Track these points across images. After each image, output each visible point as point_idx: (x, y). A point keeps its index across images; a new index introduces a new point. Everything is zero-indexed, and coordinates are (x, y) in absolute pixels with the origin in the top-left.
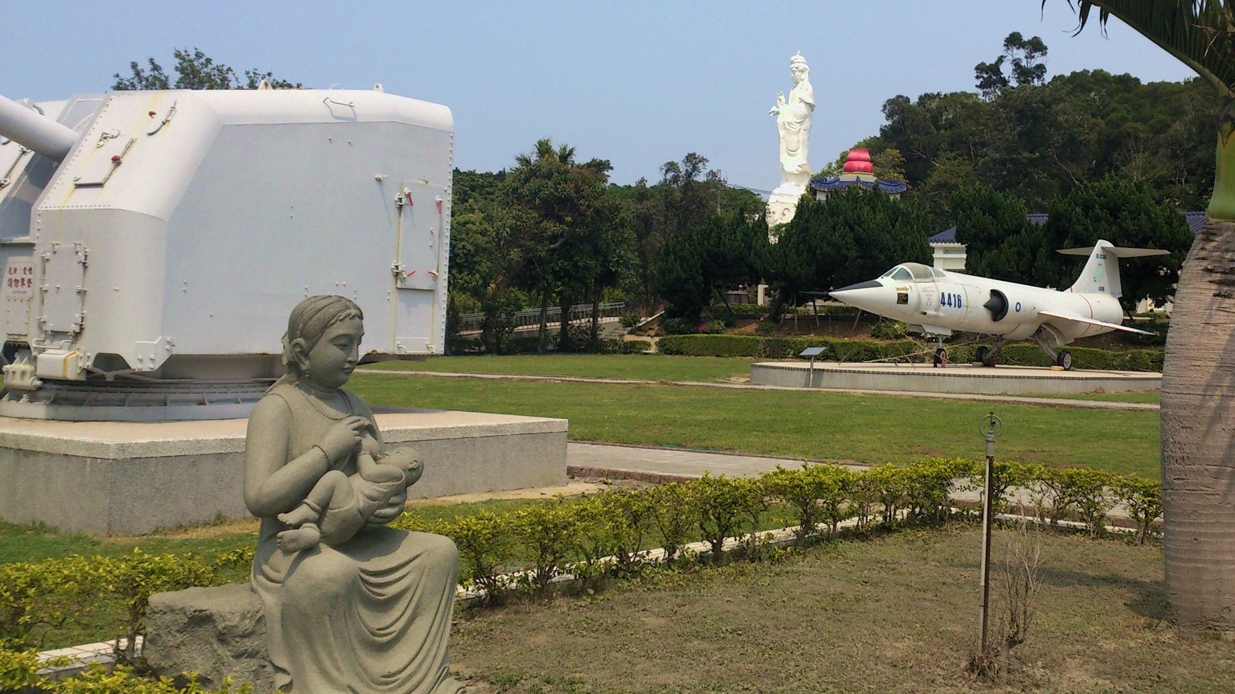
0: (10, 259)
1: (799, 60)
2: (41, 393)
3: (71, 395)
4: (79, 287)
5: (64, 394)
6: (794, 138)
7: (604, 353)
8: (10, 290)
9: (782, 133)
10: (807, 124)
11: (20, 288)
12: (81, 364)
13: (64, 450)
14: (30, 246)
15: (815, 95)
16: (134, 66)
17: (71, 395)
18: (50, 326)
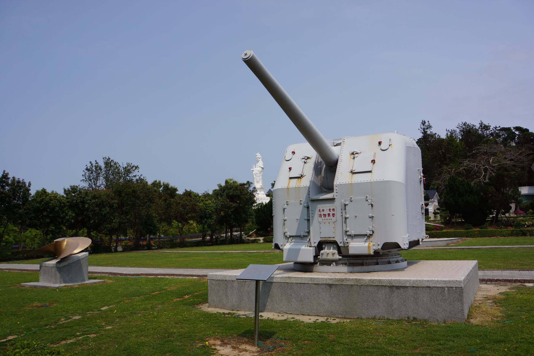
0: (319, 206)
1: (259, 155)
2: (340, 262)
3: (355, 261)
4: (371, 215)
5: (352, 261)
6: (258, 178)
7: (245, 243)
8: (320, 219)
9: (255, 176)
10: (262, 174)
11: (330, 217)
12: (375, 248)
13: (427, 284)
14: (333, 200)
15: (264, 165)
16: (91, 162)
17: (355, 261)
18: (288, 234)
